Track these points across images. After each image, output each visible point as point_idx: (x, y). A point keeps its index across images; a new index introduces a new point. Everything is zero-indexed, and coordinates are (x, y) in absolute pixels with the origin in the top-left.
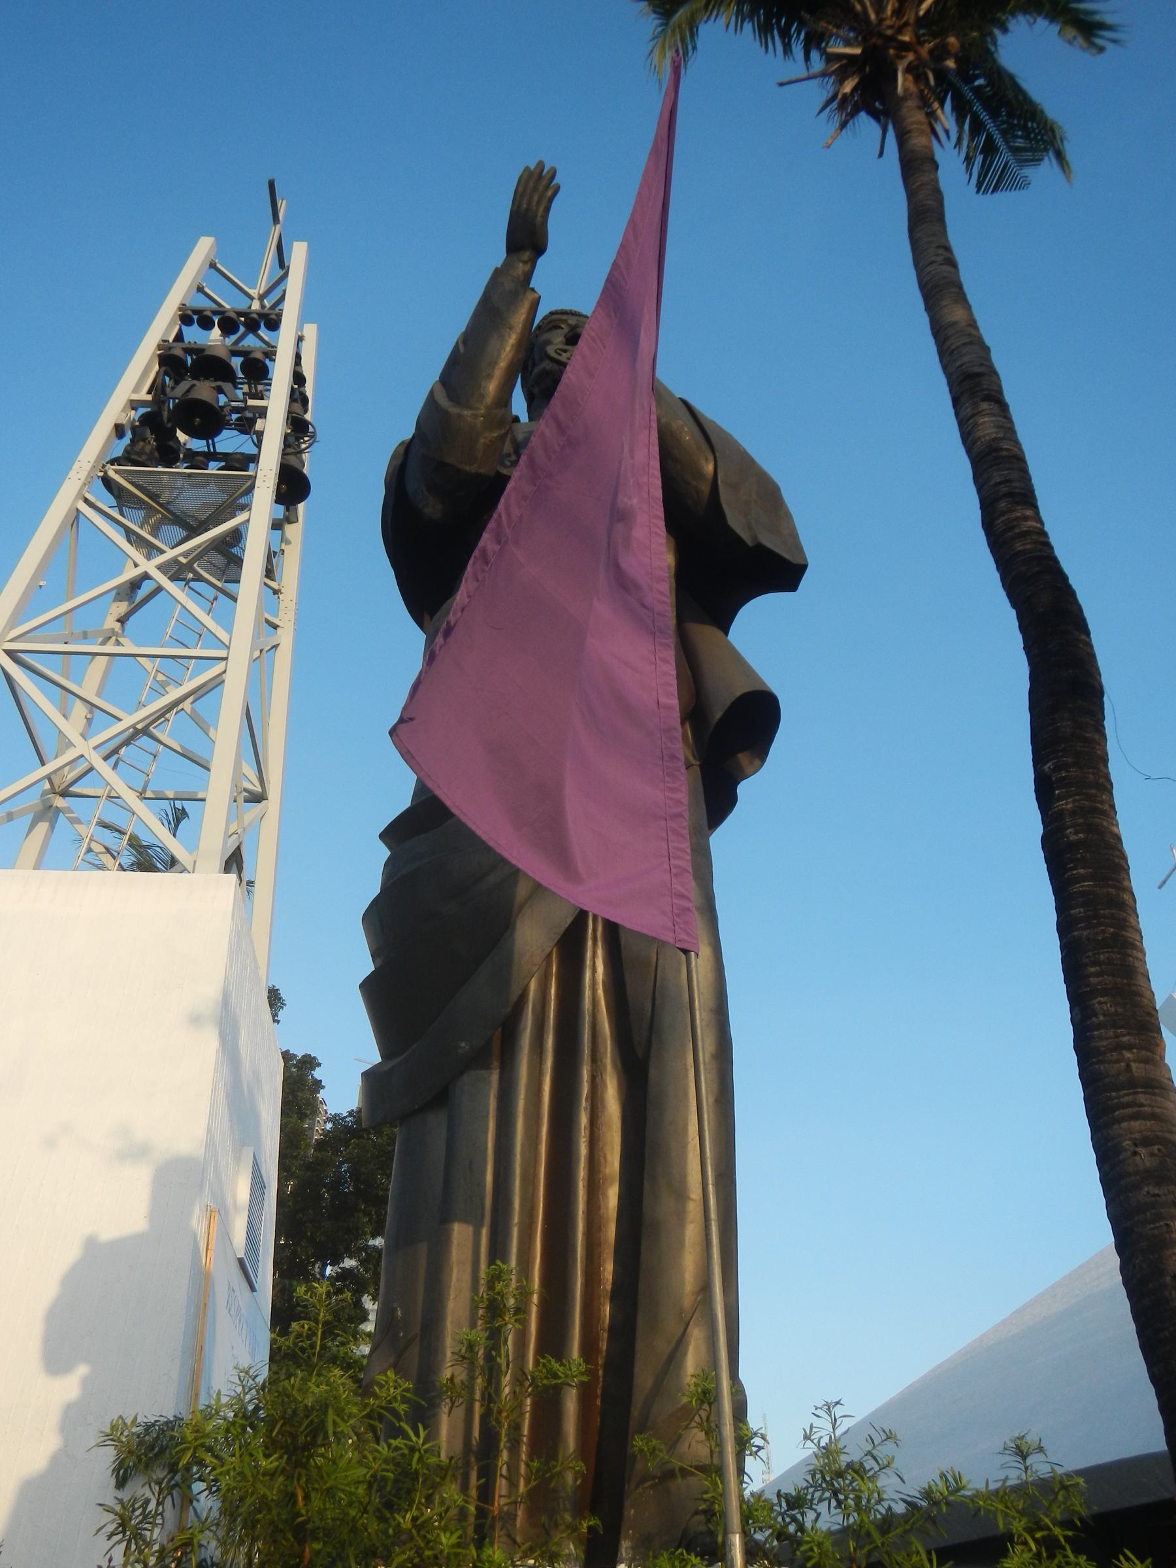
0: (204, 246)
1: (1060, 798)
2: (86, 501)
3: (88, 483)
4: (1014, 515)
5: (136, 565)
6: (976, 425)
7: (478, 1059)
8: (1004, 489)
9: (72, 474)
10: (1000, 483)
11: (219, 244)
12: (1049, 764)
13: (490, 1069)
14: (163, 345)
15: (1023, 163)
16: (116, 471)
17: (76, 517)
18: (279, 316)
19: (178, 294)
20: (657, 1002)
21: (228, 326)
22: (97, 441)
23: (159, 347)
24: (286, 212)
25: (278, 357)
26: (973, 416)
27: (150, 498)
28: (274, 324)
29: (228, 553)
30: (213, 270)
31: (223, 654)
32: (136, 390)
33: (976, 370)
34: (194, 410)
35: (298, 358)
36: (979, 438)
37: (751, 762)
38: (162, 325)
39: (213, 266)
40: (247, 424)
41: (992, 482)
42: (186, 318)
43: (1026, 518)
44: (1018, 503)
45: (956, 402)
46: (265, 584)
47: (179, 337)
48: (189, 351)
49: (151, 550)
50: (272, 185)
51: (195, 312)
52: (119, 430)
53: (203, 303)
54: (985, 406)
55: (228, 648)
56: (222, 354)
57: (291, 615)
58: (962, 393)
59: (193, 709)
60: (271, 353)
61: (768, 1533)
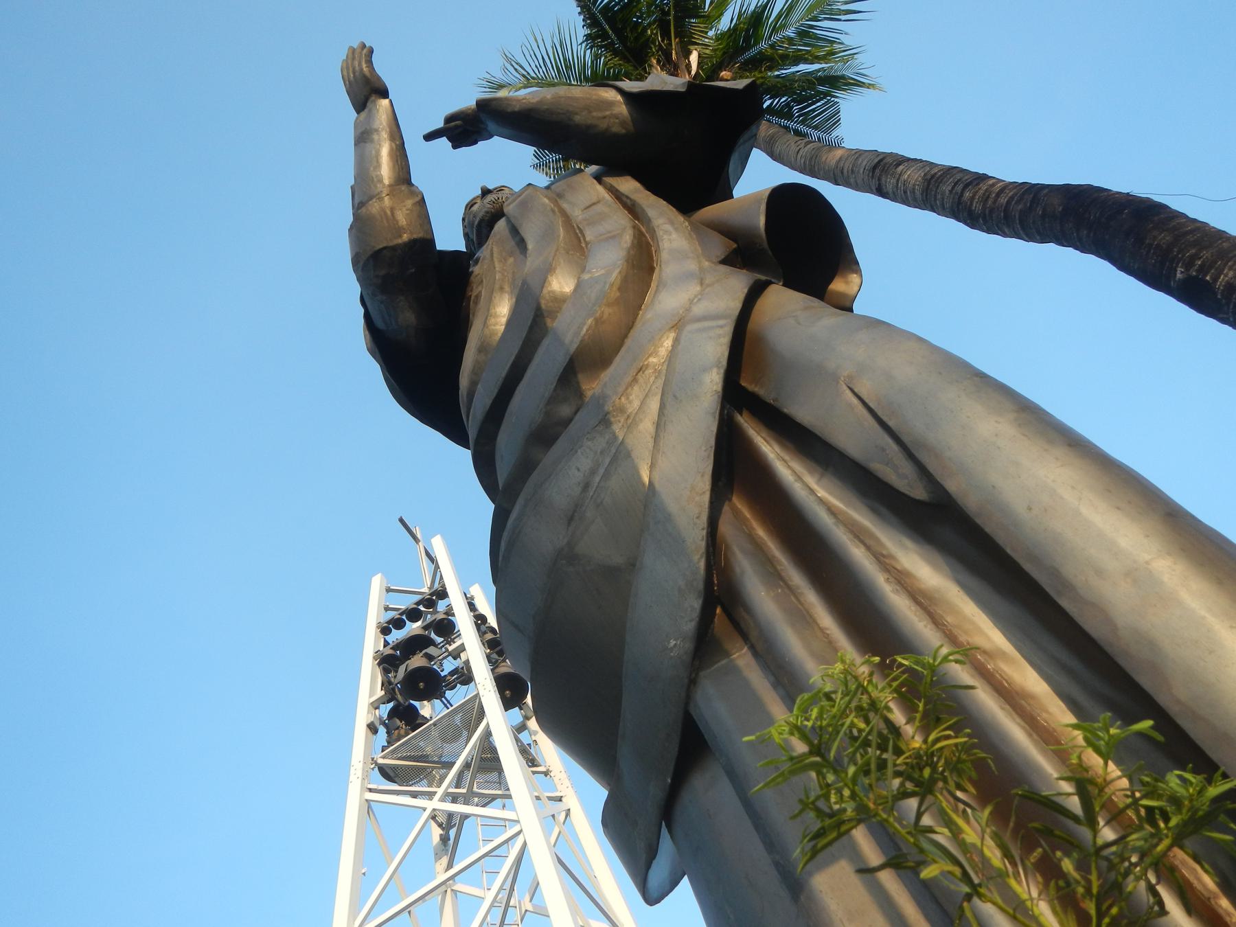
0: (377, 583)
1: (1215, 279)
2: (370, 790)
3: (366, 777)
5: (424, 809)
7: (705, 647)
8: (959, 188)
9: (352, 778)
12: (1179, 270)
13: (727, 654)
15: (829, 130)
16: (384, 757)
17: (369, 807)
18: (444, 586)
19: (374, 616)
20: (891, 423)
21: (414, 615)
22: (361, 747)
23: (375, 659)
24: (422, 534)
25: (456, 611)
28: (442, 594)
29: (488, 761)
31: (516, 829)
32: (371, 694)
34: (414, 673)
35: (472, 606)
37: (847, 283)
38: (372, 643)
39: (389, 590)
40: (465, 676)
42: (385, 631)
43: (993, 185)
45: (881, 192)
46: (534, 773)
47: (386, 644)
49: (430, 795)
50: (401, 520)
51: (389, 622)
52: (372, 728)
55: (518, 821)
56: (420, 632)
57: (567, 783)
58: (879, 179)
59: (534, 906)
60: (449, 612)
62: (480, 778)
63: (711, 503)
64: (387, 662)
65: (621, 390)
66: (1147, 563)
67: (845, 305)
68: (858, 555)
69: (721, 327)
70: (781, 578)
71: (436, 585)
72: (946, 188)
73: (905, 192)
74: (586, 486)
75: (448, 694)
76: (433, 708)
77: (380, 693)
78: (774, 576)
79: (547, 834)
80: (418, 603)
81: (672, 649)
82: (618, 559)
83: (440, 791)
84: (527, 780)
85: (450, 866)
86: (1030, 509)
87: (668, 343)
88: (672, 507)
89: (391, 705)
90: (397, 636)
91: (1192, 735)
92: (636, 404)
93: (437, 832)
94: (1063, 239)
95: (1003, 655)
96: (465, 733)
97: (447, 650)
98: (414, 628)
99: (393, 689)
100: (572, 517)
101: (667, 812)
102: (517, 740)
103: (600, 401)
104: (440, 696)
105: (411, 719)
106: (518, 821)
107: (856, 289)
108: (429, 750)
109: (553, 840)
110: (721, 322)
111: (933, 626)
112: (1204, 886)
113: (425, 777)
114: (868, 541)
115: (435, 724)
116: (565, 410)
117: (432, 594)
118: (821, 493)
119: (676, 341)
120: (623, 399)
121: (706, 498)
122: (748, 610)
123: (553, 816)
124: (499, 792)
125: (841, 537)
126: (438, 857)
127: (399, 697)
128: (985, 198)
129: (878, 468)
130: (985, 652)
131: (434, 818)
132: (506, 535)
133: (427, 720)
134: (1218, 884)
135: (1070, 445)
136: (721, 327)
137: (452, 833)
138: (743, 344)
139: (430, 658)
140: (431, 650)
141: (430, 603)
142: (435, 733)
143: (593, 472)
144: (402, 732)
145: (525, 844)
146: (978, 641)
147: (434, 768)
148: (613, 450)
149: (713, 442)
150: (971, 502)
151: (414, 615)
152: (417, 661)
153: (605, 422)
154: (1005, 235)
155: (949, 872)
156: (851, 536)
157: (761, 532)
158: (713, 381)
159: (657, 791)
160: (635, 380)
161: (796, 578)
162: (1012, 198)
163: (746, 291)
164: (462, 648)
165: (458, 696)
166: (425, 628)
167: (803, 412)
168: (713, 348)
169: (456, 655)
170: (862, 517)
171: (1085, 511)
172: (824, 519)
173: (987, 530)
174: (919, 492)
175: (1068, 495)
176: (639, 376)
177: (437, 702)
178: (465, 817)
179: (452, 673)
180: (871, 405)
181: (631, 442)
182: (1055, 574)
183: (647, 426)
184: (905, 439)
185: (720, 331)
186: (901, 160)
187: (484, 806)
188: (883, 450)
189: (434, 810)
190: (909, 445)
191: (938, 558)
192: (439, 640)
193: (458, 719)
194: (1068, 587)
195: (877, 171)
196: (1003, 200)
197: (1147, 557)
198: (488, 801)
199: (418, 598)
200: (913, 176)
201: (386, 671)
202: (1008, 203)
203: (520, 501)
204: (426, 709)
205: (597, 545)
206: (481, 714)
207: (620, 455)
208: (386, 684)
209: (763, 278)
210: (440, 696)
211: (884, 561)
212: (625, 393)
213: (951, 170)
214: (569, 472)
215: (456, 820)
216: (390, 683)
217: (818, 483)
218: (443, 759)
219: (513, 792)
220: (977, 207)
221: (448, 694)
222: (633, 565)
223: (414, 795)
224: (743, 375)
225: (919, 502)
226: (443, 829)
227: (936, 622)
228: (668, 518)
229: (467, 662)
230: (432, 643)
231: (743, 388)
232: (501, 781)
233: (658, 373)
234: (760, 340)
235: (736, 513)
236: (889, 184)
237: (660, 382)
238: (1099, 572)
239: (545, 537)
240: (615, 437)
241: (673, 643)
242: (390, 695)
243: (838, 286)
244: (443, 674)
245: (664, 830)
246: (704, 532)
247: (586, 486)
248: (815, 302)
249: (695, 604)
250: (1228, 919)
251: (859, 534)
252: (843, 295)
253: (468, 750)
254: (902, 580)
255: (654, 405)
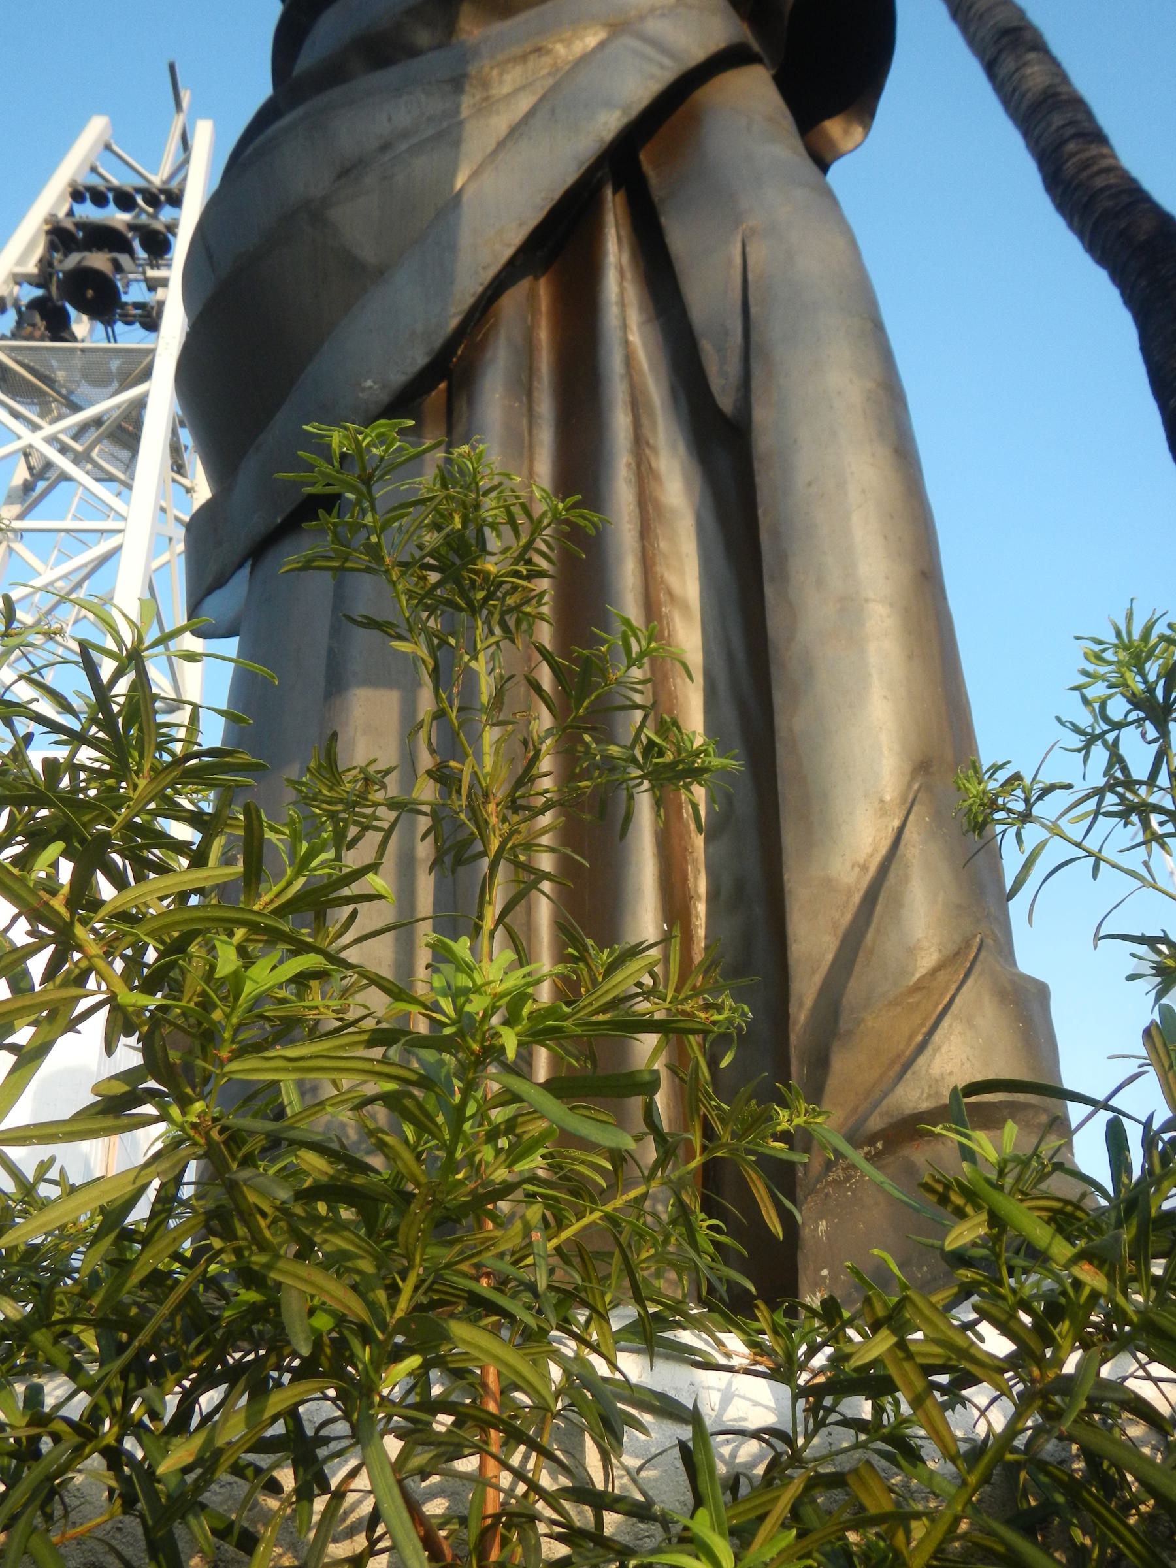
0: (96, 127)
4: (1087, 155)
5: (19, 438)
6: (1023, 77)
8: (1070, 131)
10: (1064, 126)
11: (114, 123)
14: (51, 219)
18: (182, 191)
19: (70, 168)
20: (753, 310)
21: (125, 201)
23: (46, 222)
26: (1017, 70)
27: (40, 379)
28: (175, 200)
29: (126, 433)
30: (108, 154)
32: (21, 261)
33: (1015, 24)
34: (83, 275)
36: (1029, 90)
37: (846, 132)
38: (51, 200)
39: (108, 147)
40: (150, 319)
41: (1054, 127)
42: (77, 195)
43: (1104, 156)
44: (1091, 142)
45: (991, 68)
46: (174, 480)
47: (70, 213)
48: (80, 226)
49: (35, 427)
50: (172, 68)
53: (94, 181)
54: (1032, 56)
56: (121, 227)
58: (1000, 52)
60: (172, 228)
61: (564, 1481)
62: (106, 446)
63: (511, 262)
64: (60, 237)
65: (500, 57)
66: (867, 600)
67: (822, 161)
68: (620, 422)
69: (662, 66)
70: (529, 393)
71: (174, 185)
72: (1058, 120)
73: (1014, 90)
74: (385, 147)
75: (119, 327)
76: (92, 331)
77: (31, 268)
78: (524, 387)
79: (153, 553)
80: (139, 190)
81: (363, 390)
82: (368, 254)
83: (49, 430)
84: (162, 481)
85: (21, 517)
86: (810, 484)
87: (591, 39)
88: (466, 237)
89: (39, 292)
90: (88, 212)
91: (778, 762)
92: (506, 89)
93: (21, 474)
94: (1119, 277)
95: (685, 607)
96: (116, 385)
97: (144, 273)
98: (119, 218)
99: (51, 275)
100: (349, 172)
101: (260, 550)
102: (174, 433)
103: (466, 56)
104: (109, 323)
105: (58, 327)
106: (125, 519)
107: (850, 146)
108: (60, 375)
109: (155, 564)
110: (667, 62)
111: (637, 535)
112: (696, 886)
113: (39, 404)
114: (645, 421)
115: (83, 350)
116: (423, 37)
117: (162, 191)
118: (634, 337)
119: (602, 45)
120: (495, 72)
121: (508, 253)
122: (471, 401)
123: (170, 539)
124: (122, 476)
125: (617, 393)
126: (10, 500)
127: (54, 290)
128: (1086, 165)
129: (707, 347)
130: (670, 593)
131: (26, 455)
132: (261, 139)
133: (74, 338)
134: (707, 893)
135: (896, 451)
136: (662, 66)
137: (41, 485)
138: (671, 111)
139: (118, 268)
140: (124, 259)
141: (153, 199)
142: (78, 361)
143: (405, 134)
144: (37, 334)
145: (119, 548)
146: (673, 580)
147: (55, 400)
148: (445, 125)
149: (557, 195)
150: (764, 441)
151: (125, 201)
152: (99, 261)
153: (457, 83)
154: (1070, 225)
155: (424, 661)
156: (628, 398)
157: (544, 335)
158: (608, 124)
159: (260, 522)
160: (524, 58)
161: (545, 406)
162: (1108, 187)
163: (722, 45)
164: (164, 283)
165: (130, 337)
166: (132, 227)
167: (680, 238)
168: (636, 86)
169: (153, 285)
170: (656, 391)
171: (856, 519)
172: (614, 363)
173: (758, 479)
174: (726, 402)
175: (854, 494)
176: (532, 57)
177: (100, 327)
178: (65, 477)
179: (137, 305)
180: (750, 277)
181: (470, 129)
182: (782, 558)
183: (500, 123)
184: (754, 336)
185: (656, 71)
186: (1038, 45)
187: (97, 480)
188: (726, 334)
189: (31, 446)
190: (753, 346)
191: (698, 482)
192: (141, 254)
193: (115, 365)
194: (783, 577)
195: (1005, 40)
196: (1099, 182)
197: (871, 595)
198: (105, 478)
199: (141, 183)
200: (1035, 77)
201: (52, 247)
202: (1103, 189)
203: (300, 111)
204: (81, 325)
205: (357, 222)
206: (146, 375)
207: (448, 135)
208: (46, 264)
209: (756, 47)
210: (109, 323)
211: (640, 443)
212: (503, 66)
213: (1078, 103)
214: (378, 114)
215: (53, 475)
216: (50, 265)
217: (642, 325)
218: (73, 398)
219: (136, 484)
220: (1070, 167)
221: (119, 327)
222: (380, 273)
223: (16, 415)
224: (649, 146)
225: (719, 412)
226: (32, 474)
227: (645, 532)
228: (452, 247)
229: (161, 304)
230: (131, 252)
231: (638, 164)
232: (129, 466)
233: (555, 68)
234: (695, 120)
235: (532, 296)
236: (1007, 65)
237: (550, 81)
238: (820, 583)
239: (302, 173)
240: (457, 110)
241: (369, 383)
242: (42, 279)
243: (834, 127)
244: (124, 298)
245: (249, 563)
246: (480, 289)
247: (385, 147)
248: (787, 122)
249: (419, 358)
250: (693, 919)
251: (636, 405)
252: (830, 143)
253: (109, 404)
254: (644, 477)
255: (524, 103)
